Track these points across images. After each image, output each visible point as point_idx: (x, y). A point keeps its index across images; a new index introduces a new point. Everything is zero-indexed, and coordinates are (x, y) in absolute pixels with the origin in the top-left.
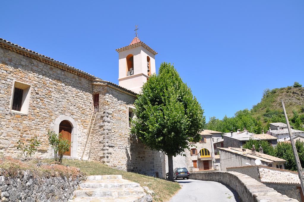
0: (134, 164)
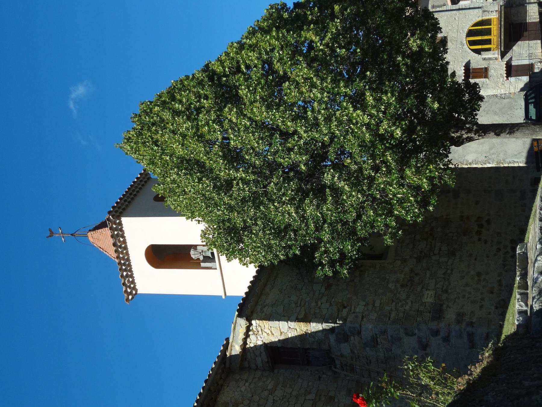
0: (499, 250)
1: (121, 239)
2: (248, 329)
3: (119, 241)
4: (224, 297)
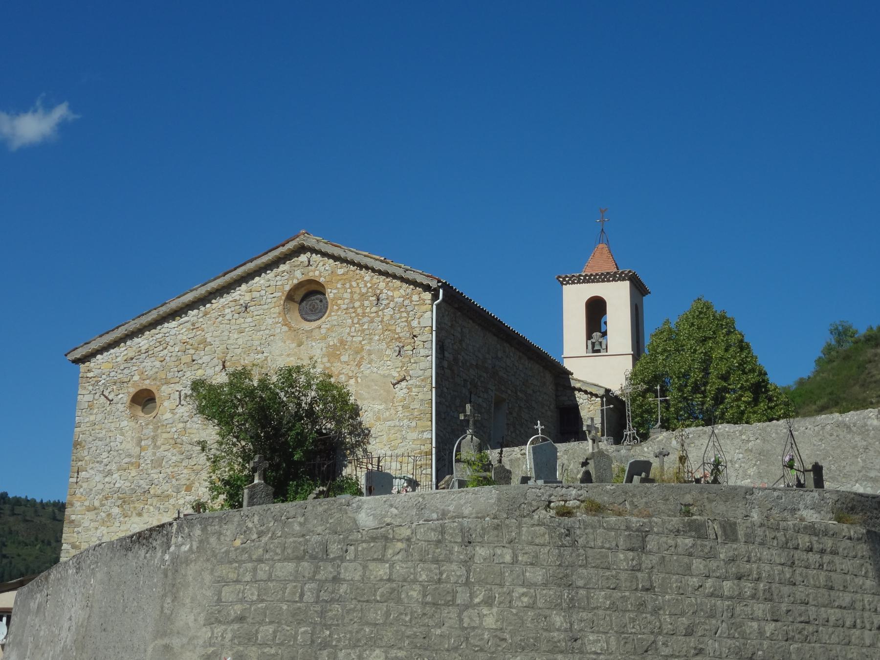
1: (611, 279)
2: (596, 396)
3: (610, 277)
4: (562, 356)
